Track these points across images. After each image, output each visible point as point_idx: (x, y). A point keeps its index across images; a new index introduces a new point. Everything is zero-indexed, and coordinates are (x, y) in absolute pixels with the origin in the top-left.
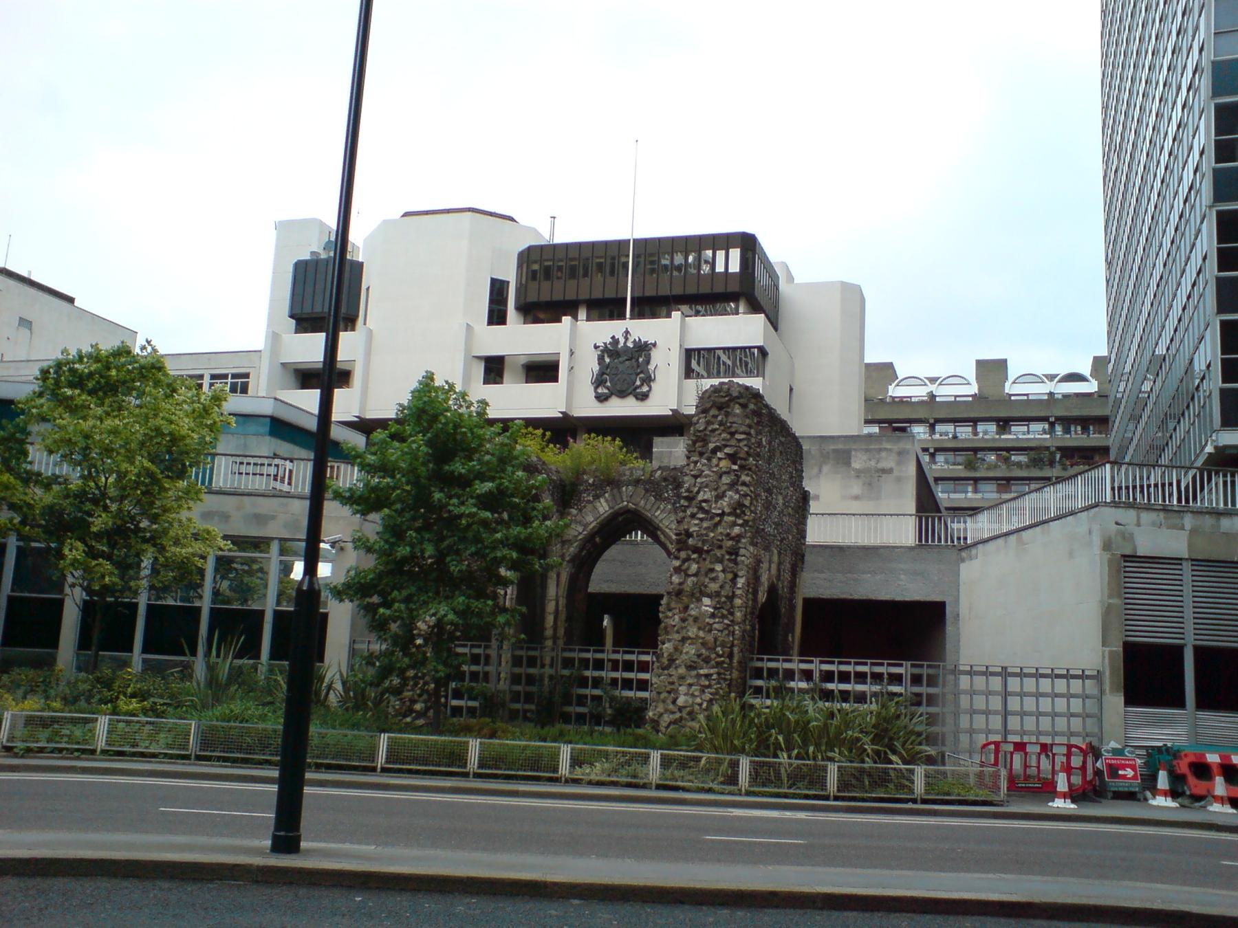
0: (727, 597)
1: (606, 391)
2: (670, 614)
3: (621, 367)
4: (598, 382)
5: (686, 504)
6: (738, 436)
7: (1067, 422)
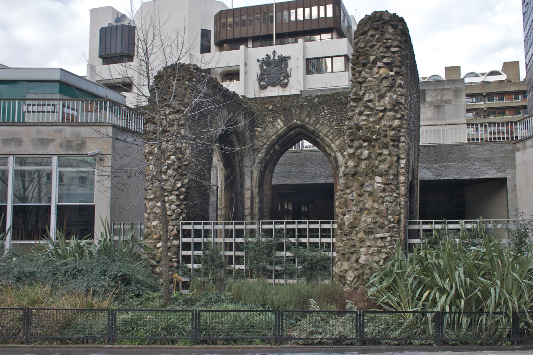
0: (394, 175)
1: (265, 83)
2: (348, 191)
3: (272, 71)
4: (261, 79)
5: (354, 104)
6: (392, 49)
7: (490, 96)
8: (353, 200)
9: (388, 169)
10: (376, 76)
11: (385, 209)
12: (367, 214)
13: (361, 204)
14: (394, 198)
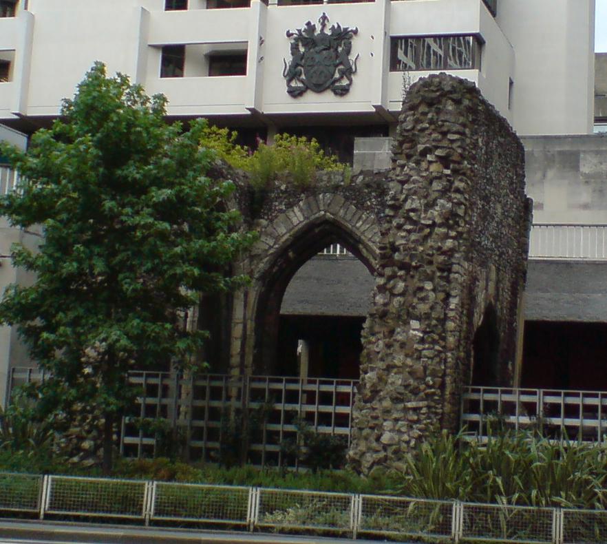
0: (438, 319)
1: (300, 85)
2: (373, 339)
4: (292, 75)
5: (391, 213)
6: (451, 137)
8: (378, 353)
9: (429, 311)
10: (424, 174)
11: (422, 368)
12: (395, 374)
13: (390, 358)
14: (436, 353)
